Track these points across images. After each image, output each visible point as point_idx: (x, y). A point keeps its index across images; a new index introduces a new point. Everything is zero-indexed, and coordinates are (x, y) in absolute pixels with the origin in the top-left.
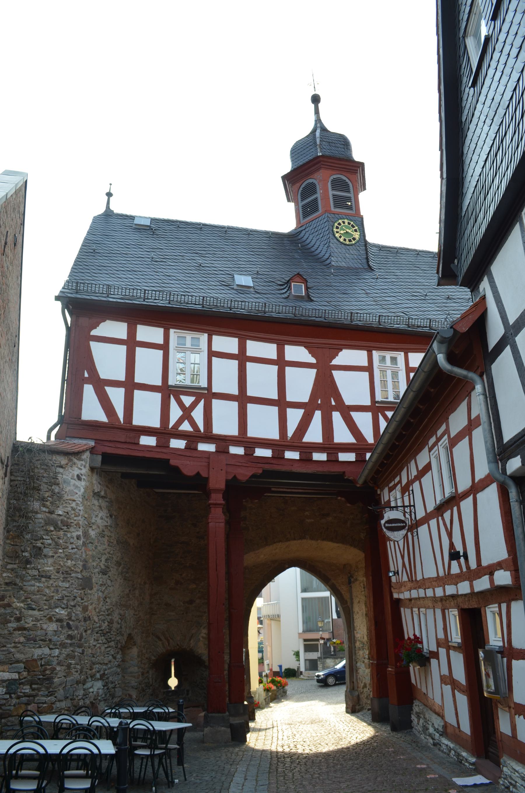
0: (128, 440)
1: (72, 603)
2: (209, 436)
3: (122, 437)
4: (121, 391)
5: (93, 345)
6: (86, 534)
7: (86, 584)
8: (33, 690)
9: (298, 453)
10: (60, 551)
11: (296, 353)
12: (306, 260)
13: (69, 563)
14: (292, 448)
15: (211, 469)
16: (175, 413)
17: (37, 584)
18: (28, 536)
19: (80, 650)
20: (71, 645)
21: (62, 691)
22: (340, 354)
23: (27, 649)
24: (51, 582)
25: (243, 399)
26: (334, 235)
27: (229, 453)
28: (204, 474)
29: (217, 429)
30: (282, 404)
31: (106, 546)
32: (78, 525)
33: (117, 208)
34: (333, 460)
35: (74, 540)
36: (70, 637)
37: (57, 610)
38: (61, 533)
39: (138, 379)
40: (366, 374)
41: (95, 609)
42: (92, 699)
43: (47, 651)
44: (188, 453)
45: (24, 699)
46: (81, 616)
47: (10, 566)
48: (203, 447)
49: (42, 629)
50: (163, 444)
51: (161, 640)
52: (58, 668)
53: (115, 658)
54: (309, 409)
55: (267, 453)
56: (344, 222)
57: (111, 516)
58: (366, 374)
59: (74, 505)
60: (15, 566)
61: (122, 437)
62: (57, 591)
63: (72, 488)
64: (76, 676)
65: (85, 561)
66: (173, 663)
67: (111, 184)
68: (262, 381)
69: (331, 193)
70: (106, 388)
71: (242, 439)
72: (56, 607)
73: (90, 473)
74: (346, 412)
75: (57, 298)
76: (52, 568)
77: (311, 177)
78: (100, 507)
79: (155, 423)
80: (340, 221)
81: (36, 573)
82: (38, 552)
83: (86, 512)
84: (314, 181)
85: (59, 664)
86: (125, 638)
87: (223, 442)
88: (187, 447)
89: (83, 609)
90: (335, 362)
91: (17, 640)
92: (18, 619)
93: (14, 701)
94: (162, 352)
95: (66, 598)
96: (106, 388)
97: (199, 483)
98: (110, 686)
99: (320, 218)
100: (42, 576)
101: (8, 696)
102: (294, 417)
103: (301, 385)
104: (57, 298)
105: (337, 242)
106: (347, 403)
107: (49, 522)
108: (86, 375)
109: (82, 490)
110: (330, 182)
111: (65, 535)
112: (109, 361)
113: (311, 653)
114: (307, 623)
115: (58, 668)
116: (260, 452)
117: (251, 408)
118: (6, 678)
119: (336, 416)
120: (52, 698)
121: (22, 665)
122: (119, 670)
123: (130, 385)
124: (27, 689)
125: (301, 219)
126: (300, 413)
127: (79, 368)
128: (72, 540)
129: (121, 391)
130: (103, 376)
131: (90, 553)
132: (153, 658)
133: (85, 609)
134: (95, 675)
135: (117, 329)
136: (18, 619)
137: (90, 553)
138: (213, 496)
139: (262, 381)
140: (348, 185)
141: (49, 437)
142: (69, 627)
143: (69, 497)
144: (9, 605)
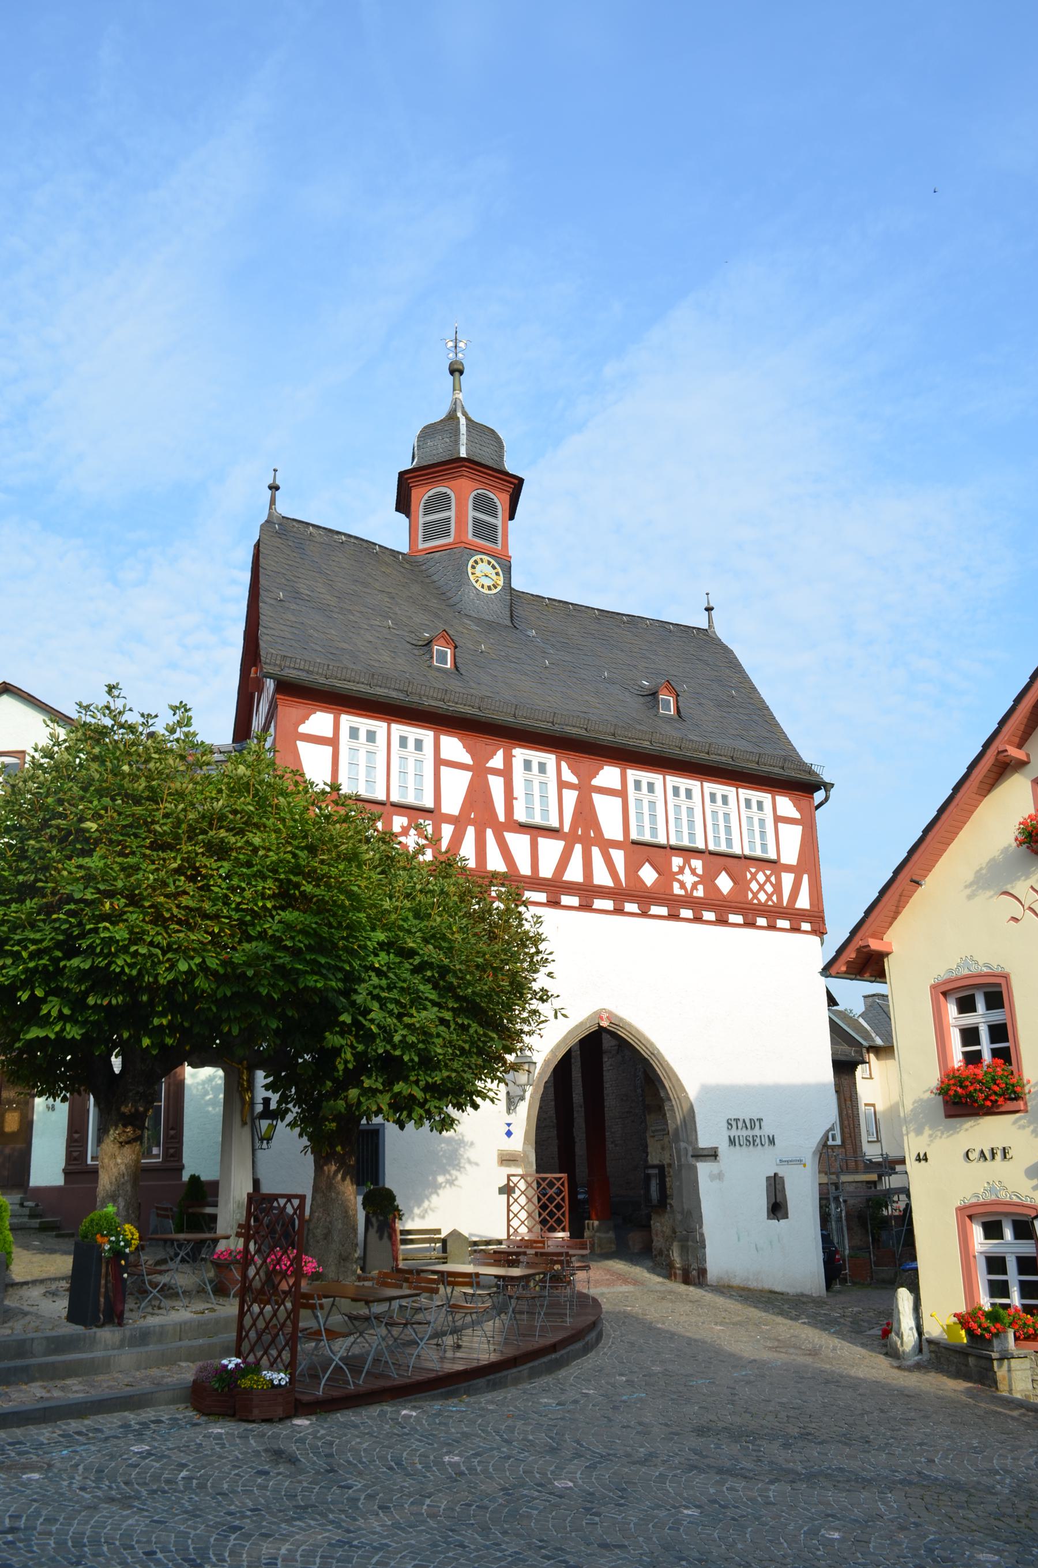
22: (313, 717)
33: (285, 508)
40: (618, 801)
58: (618, 801)
67: (275, 470)
74: (605, 846)
90: (303, 729)
106: (606, 836)
119: (596, 851)
140: (495, 507)
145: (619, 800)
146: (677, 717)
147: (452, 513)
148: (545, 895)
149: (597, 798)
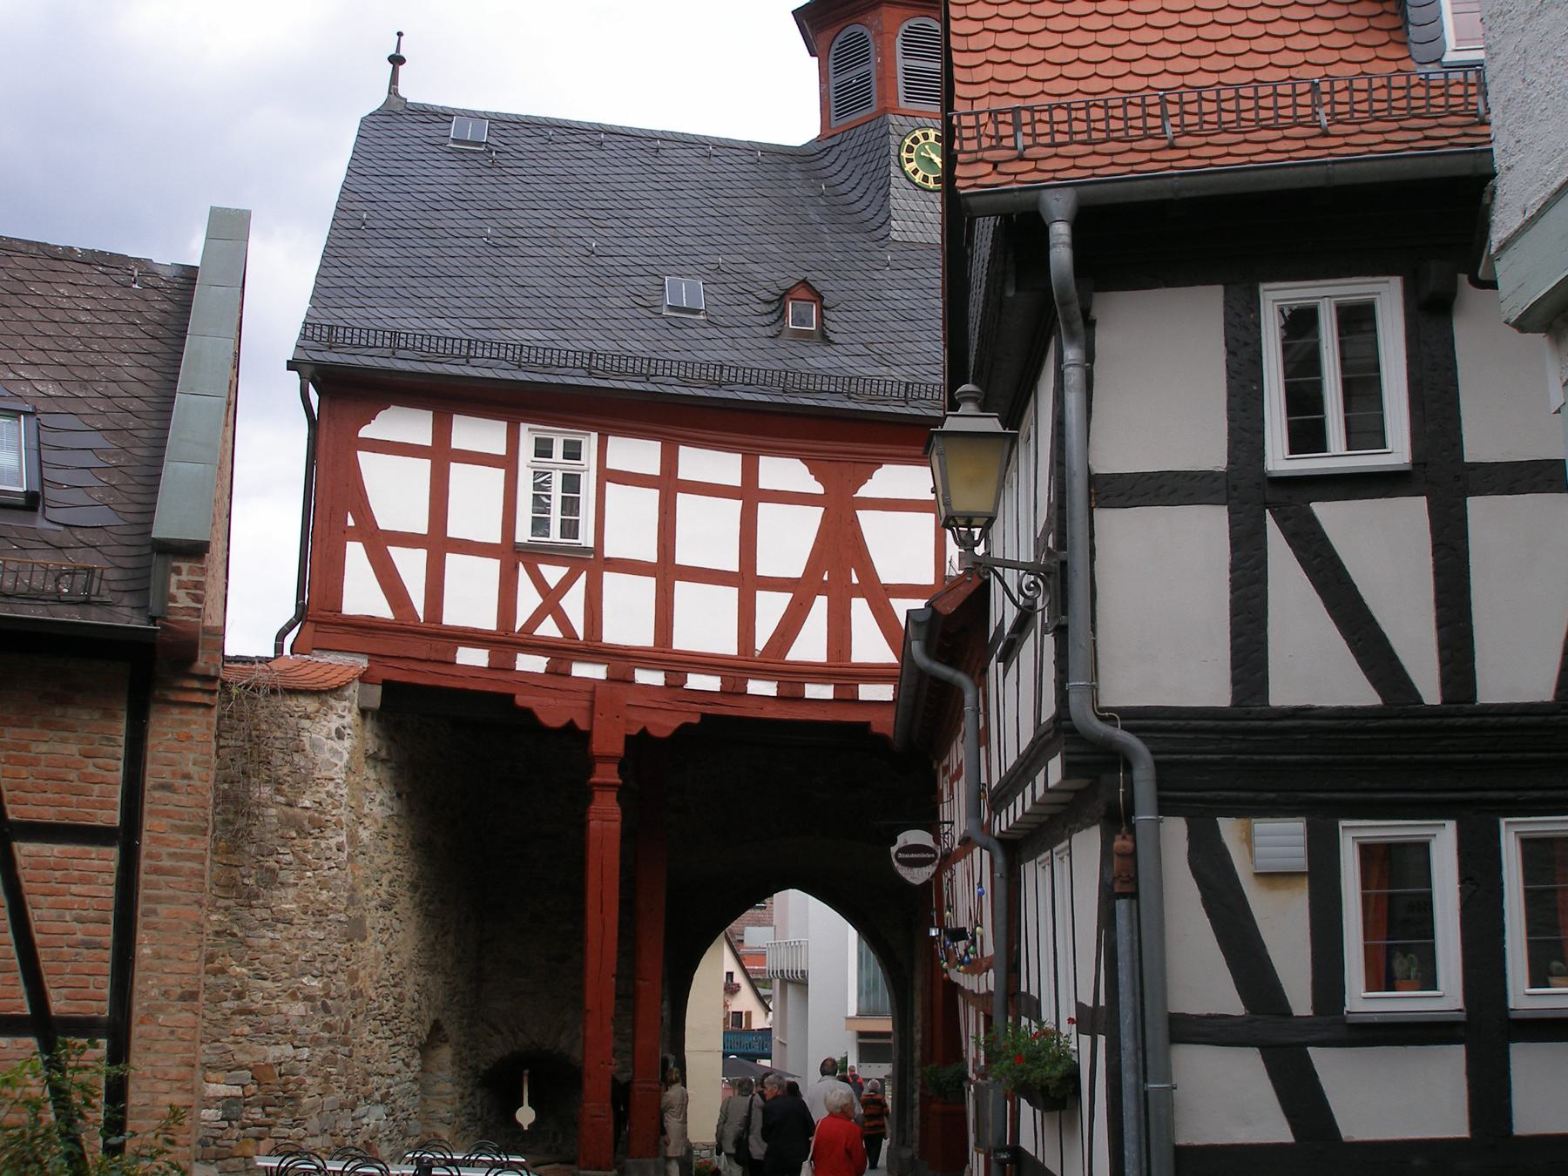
0: (434, 656)
1: (331, 967)
2: (594, 650)
3: (421, 649)
4: (421, 555)
5: (364, 457)
6: (353, 839)
7: (355, 931)
8: (268, 1115)
9: (775, 684)
10: (309, 874)
11: (783, 472)
12: (834, 228)
13: (325, 895)
14: (762, 673)
15: (597, 716)
16: (528, 600)
17: (271, 935)
18: (253, 849)
19: (346, 1050)
20: (330, 1040)
21: (315, 1119)
22: (878, 474)
23: (256, 1046)
24: (294, 930)
25: (666, 571)
26: (902, 168)
27: (633, 682)
28: (582, 725)
29: (612, 634)
30: (747, 581)
31: (389, 856)
32: (338, 824)
33: (415, 90)
34: (846, 698)
35: (333, 853)
36: (328, 1027)
37: (305, 980)
38: (311, 841)
39: (454, 531)
41: (371, 976)
42: (366, 1138)
43: (288, 1050)
44: (554, 682)
45: (253, 1130)
46: (345, 991)
47: (220, 903)
48: (580, 670)
49: (279, 1013)
50: (501, 665)
51: (500, 1033)
52: (309, 1080)
53: (407, 1065)
54: (801, 591)
55: (712, 683)
56: (926, 136)
57: (399, 795)
59: (330, 787)
60: (231, 903)
61: (421, 649)
62: (305, 946)
63: (328, 755)
64: (340, 1095)
65: (353, 889)
66: (525, 1079)
67: (400, 34)
68: (708, 533)
69: (900, 63)
70: (390, 549)
71: (663, 655)
72: (304, 975)
73: (359, 721)
75: (292, 365)
76: (294, 906)
77: (860, 19)
78: (378, 781)
79: (487, 620)
80: (918, 133)
81: (266, 914)
82: (271, 879)
83: (353, 797)
84: (866, 32)
85: (309, 1073)
86: (428, 1028)
87: (623, 659)
88: (550, 671)
89: (350, 977)
90: (865, 491)
91: (237, 1031)
92: (239, 996)
93: (236, 1132)
94: (502, 472)
95: (320, 959)
96: (390, 549)
97: (574, 737)
98: (400, 1115)
99: (873, 124)
100: (278, 921)
101: (226, 1124)
102: (771, 608)
103: (789, 538)
104: (292, 365)
105: (908, 185)
107: (288, 822)
108: (351, 522)
109: (346, 756)
110: (899, 42)
111: (317, 845)
112: (394, 490)
113: (874, 1066)
114: (867, 994)
115: (309, 1080)
116: (696, 682)
117: (682, 589)
118: (222, 1094)
120: (300, 1131)
121: (249, 1074)
122: (415, 1087)
123: (438, 543)
124: (257, 1114)
125: (833, 118)
126: (782, 600)
127: (333, 509)
128: (328, 854)
129: (421, 555)
130: (383, 524)
131: (361, 872)
132: (483, 1067)
133: (353, 977)
134: (371, 1094)
135: (414, 426)
136: (239, 996)
137: (361, 872)
138: (599, 768)
139: (708, 533)
141: (279, 648)
142: (326, 1009)
143: (325, 774)
144: (222, 971)
145: (500, 473)
146: (817, 334)
147: (872, 67)
148: (485, 652)
149: (868, 521)
